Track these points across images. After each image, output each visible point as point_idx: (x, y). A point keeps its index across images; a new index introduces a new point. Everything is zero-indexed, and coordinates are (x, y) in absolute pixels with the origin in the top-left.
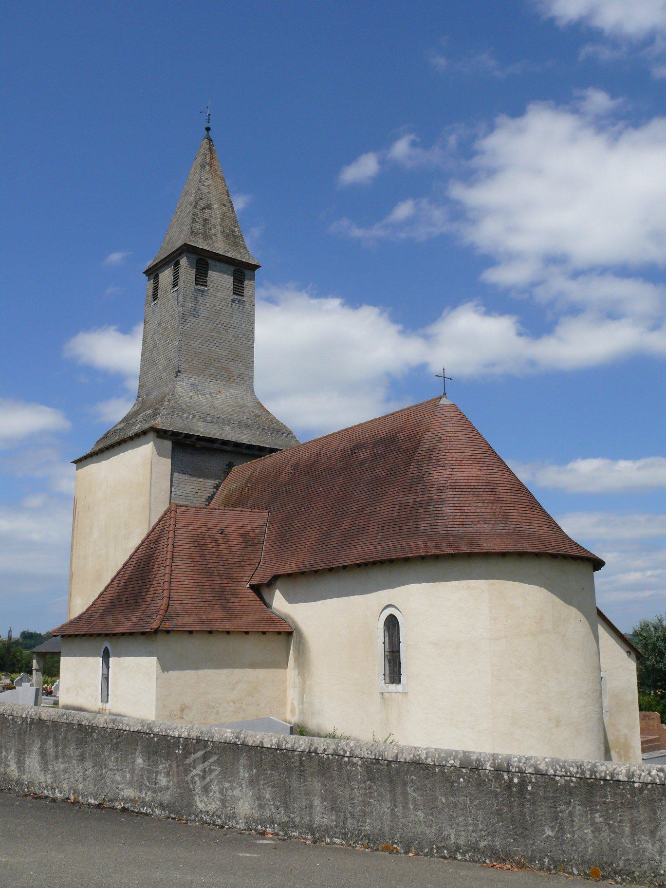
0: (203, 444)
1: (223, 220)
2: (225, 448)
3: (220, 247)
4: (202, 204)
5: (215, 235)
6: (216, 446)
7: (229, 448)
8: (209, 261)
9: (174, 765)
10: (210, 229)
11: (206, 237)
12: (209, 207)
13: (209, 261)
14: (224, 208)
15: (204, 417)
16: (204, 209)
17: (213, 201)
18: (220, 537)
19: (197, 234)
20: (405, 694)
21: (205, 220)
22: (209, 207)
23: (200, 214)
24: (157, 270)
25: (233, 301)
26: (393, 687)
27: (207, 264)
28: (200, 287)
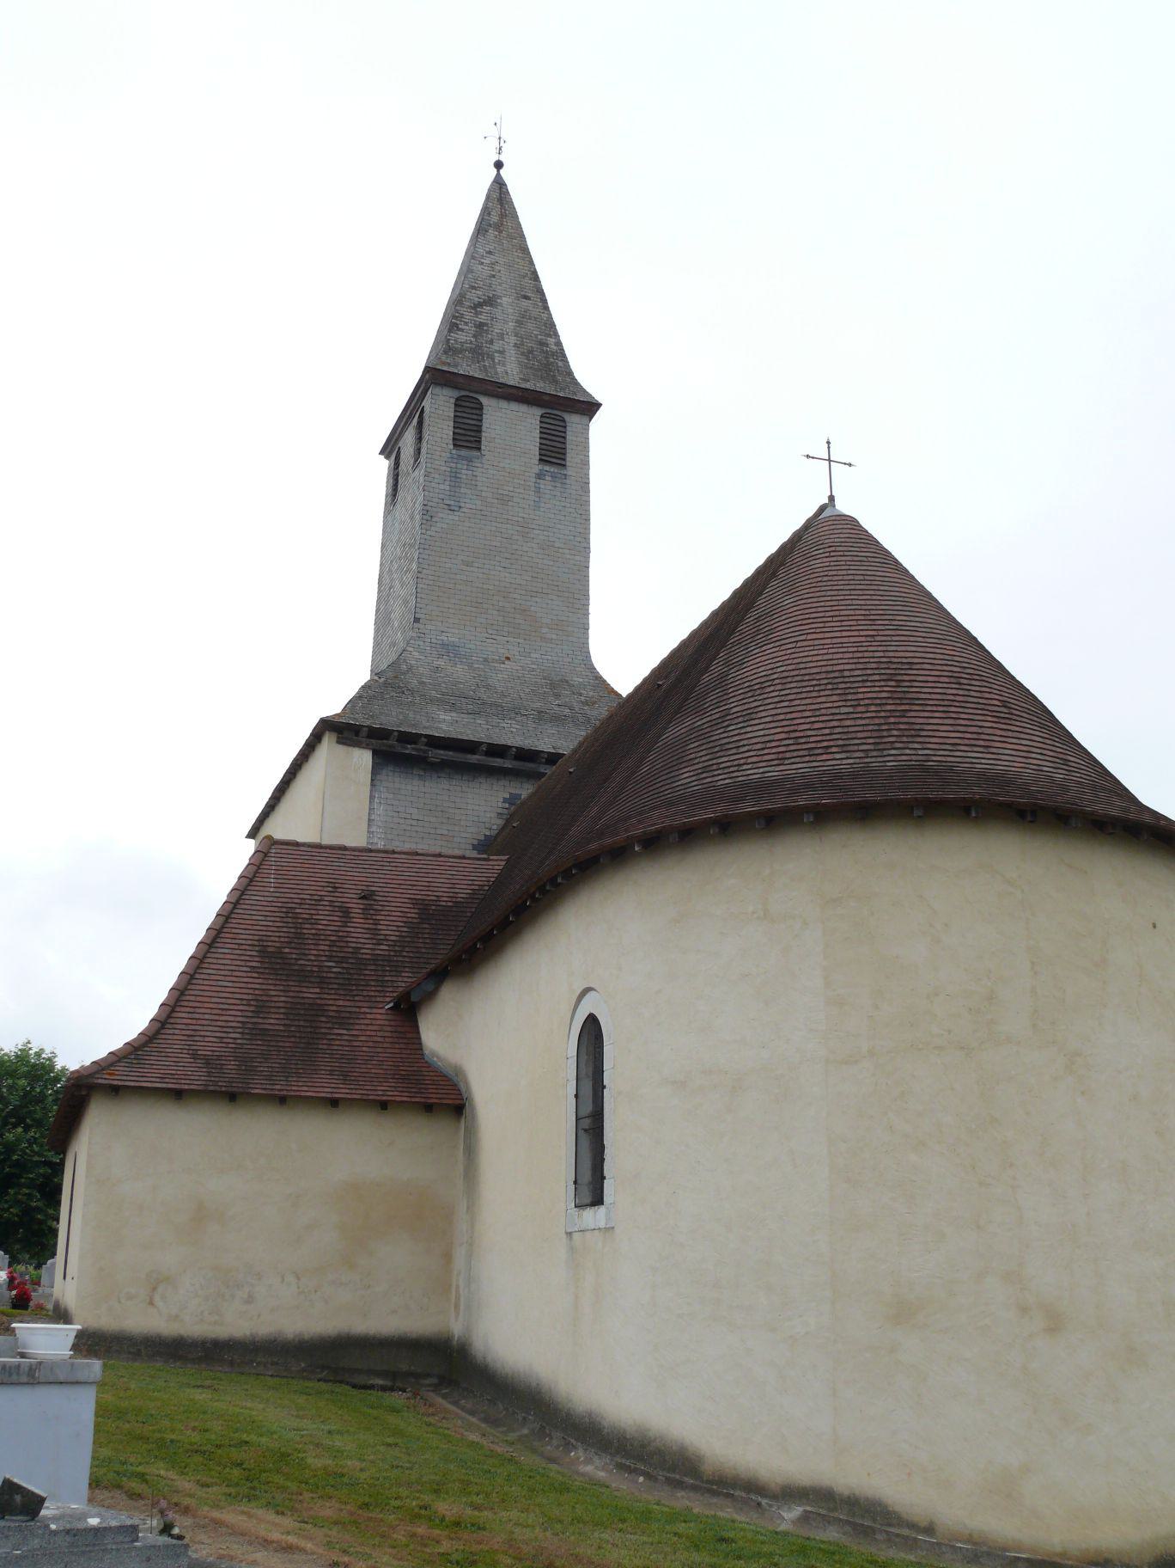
0: (443, 754)
1: (519, 323)
2: (497, 762)
3: (510, 371)
4: (474, 296)
5: (502, 352)
6: (474, 758)
7: (508, 764)
8: (484, 400)
9: (278, 1479)
10: (491, 342)
11: (478, 353)
12: (490, 301)
13: (484, 400)
14: (525, 303)
15: (452, 700)
16: (480, 305)
17: (499, 290)
18: (356, 907)
19: (461, 351)
20: (610, 1229)
21: (480, 325)
22: (490, 301)
23: (469, 316)
24: (397, 440)
25: (540, 476)
26: (594, 1217)
27: (480, 407)
28: (464, 452)
